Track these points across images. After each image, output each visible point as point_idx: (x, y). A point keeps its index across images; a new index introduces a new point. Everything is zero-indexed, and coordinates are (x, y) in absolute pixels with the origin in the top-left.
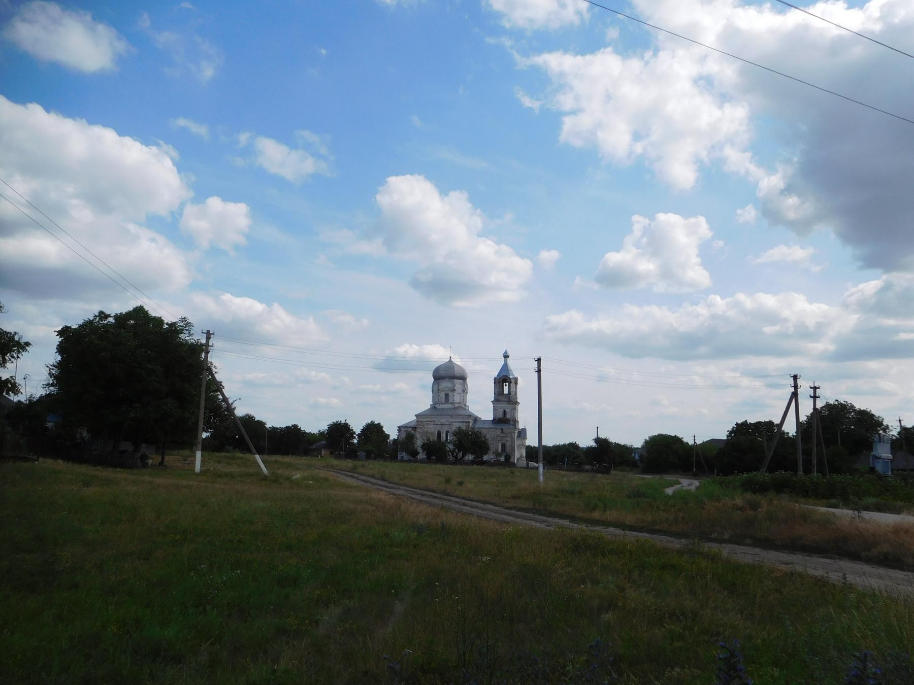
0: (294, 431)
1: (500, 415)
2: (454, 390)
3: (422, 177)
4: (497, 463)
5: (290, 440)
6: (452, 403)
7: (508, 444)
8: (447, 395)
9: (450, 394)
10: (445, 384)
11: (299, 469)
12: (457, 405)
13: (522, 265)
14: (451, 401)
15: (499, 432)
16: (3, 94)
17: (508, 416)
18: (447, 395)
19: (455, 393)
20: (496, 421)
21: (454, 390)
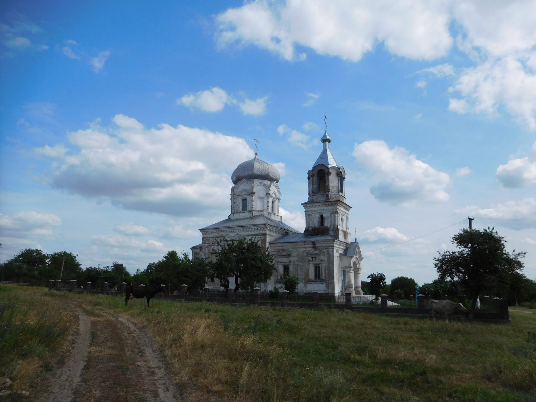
0: (65, 262)
1: (316, 223)
2: (252, 193)
3: (382, 142)
4: (274, 295)
5: (112, 281)
6: (250, 211)
7: (323, 265)
8: (244, 200)
9: (249, 198)
10: (244, 186)
11: (335, 317)
12: (255, 214)
13: (444, 177)
14: (248, 208)
15: (309, 248)
16: (534, 284)
17: (327, 224)
18: (244, 200)
19: (255, 197)
20: (310, 232)
21: (252, 193)
